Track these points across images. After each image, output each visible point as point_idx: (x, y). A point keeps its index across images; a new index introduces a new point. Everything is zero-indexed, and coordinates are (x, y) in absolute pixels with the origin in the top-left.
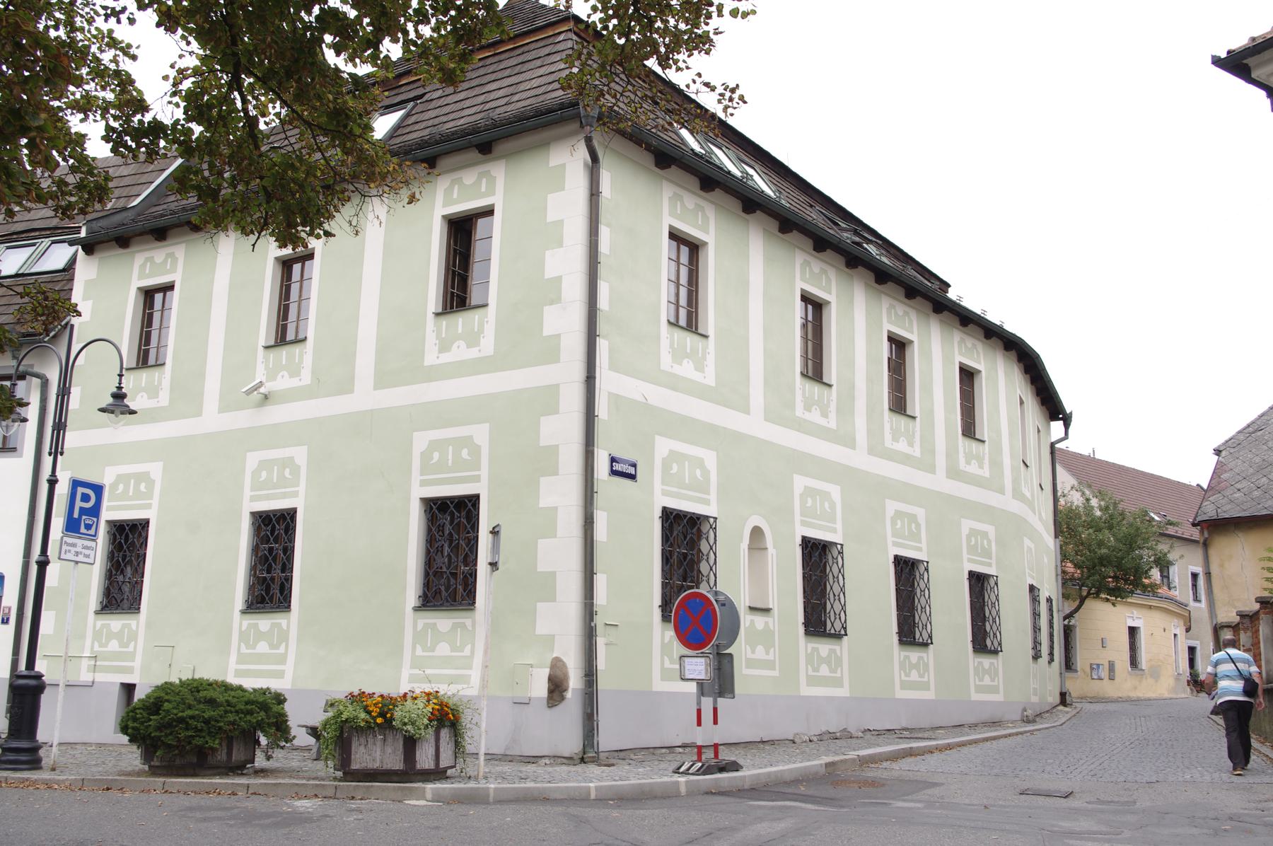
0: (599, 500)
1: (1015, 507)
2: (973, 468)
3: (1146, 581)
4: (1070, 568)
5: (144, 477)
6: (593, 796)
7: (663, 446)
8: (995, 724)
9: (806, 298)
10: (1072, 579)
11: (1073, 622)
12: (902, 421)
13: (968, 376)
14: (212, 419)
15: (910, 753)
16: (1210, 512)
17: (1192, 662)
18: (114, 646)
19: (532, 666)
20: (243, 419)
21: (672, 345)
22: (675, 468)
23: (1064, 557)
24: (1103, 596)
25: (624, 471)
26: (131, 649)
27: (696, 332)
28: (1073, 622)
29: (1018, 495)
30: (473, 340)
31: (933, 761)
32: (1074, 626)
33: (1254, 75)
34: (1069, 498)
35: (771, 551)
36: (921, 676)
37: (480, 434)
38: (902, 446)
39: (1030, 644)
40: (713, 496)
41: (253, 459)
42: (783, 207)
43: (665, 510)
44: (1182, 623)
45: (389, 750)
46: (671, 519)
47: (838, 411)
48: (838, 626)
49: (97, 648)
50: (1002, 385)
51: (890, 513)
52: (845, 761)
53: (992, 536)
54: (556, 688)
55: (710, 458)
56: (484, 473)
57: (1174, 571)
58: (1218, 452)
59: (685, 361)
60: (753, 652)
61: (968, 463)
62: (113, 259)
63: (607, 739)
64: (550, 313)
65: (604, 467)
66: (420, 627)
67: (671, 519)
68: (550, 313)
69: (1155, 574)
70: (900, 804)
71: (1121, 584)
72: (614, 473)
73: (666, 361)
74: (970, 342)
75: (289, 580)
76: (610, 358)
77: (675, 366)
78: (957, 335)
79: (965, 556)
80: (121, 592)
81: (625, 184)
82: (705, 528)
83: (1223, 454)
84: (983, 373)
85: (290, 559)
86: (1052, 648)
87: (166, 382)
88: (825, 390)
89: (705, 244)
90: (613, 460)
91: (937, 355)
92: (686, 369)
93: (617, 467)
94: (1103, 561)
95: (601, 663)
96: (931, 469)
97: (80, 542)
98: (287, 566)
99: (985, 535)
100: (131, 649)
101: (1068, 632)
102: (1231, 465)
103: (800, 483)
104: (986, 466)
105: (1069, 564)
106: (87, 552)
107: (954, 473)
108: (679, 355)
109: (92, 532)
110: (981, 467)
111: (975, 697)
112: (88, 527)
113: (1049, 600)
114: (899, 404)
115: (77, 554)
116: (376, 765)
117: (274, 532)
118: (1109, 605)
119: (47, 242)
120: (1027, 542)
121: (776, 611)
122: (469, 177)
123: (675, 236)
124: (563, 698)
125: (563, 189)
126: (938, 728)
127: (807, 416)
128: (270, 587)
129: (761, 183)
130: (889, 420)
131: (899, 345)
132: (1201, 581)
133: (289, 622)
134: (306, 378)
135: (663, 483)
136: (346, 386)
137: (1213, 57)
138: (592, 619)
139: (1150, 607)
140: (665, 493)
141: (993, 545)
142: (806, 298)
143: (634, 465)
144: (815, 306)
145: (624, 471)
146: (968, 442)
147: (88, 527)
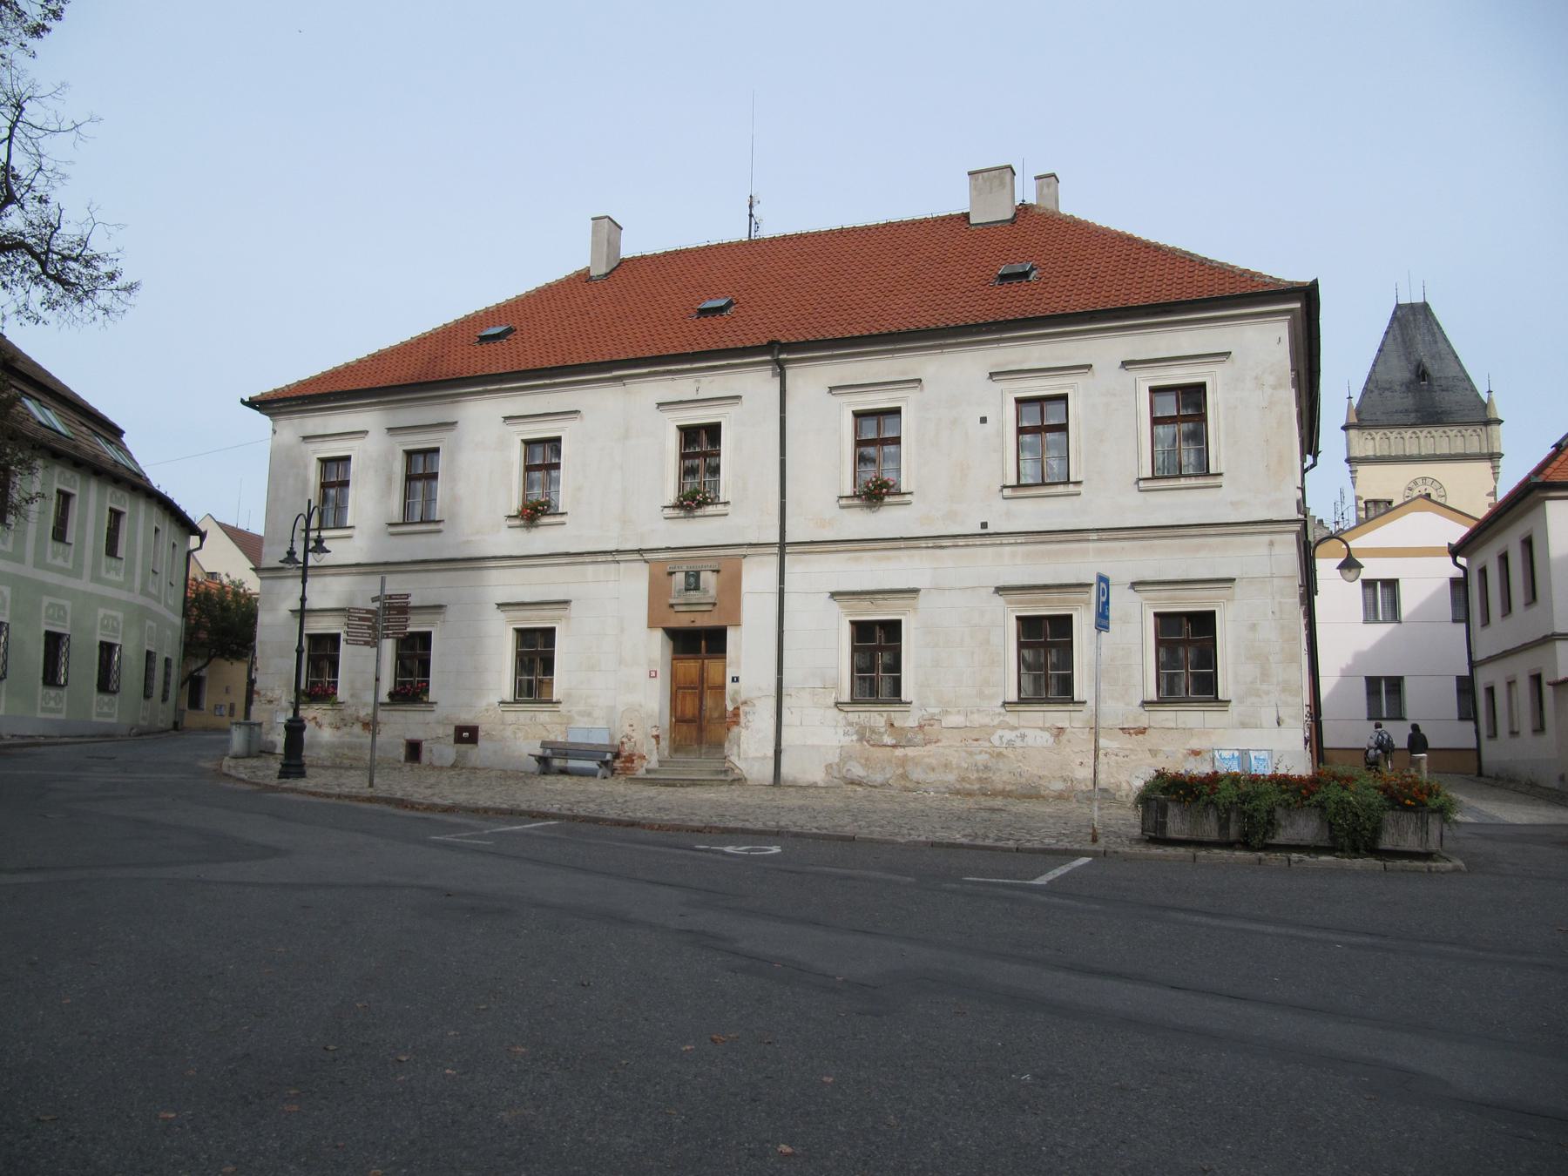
11: (203, 673)
12: (61, 546)
38: (59, 562)
74: (119, 493)
99: (115, 618)
111: (95, 718)
130: (104, 559)
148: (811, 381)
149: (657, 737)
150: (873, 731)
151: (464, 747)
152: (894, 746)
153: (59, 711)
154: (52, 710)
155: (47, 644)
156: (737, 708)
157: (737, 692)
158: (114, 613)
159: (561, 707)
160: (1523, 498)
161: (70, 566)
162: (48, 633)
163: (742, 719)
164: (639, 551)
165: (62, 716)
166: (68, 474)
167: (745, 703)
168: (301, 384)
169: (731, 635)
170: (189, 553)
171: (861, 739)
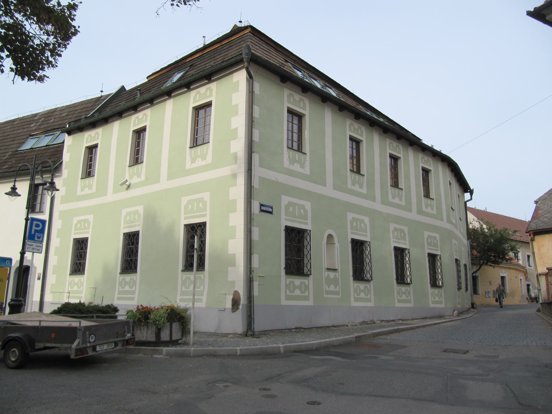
0: (254, 222)
1: (447, 226)
2: (429, 210)
3: (507, 258)
4: (475, 252)
5: (86, 221)
6: (239, 353)
7: (285, 200)
8: (440, 317)
9: (352, 139)
10: (476, 257)
11: (477, 274)
12: (397, 190)
13: (426, 172)
14: (111, 197)
15: (398, 331)
16: (533, 227)
17: (528, 290)
18: (75, 288)
19: (226, 294)
20: (125, 195)
21: (289, 157)
22: (291, 209)
23: (472, 248)
24: (489, 264)
25: (266, 209)
26: (81, 289)
27: (301, 152)
28: (477, 274)
29: (449, 221)
30: (204, 158)
31: (407, 334)
32: (478, 276)
33: (547, 18)
34: (473, 225)
35: (337, 244)
36: (407, 297)
38: (397, 201)
39: (456, 283)
40: (309, 221)
41: (124, 212)
42: (340, 100)
43: (286, 226)
44: (523, 274)
45: (149, 332)
46: (290, 231)
47: (367, 186)
48: (368, 276)
49: (70, 289)
50: (440, 176)
51: (391, 229)
52: (366, 335)
53: (438, 238)
54: (235, 303)
55: (308, 205)
56: (208, 213)
57: (520, 255)
58: (536, 202)
59: (295, 164)
60: (329, 287)
61: (427, 208)
62: (78, 136)
63: (258, 326)
64: (233, 143)
65: (258, 208)
66: (184, 278)
67: (290, 231)
68: (233, 143)
69: (511, 254)
70: (383, 357)
71: (497, 259)
72: (262, 211)
73: (286, 164)
74: (426, 158)
75: (136, 260)
76: (260, 161)
77: (291, 166)
78: (420, 155)
79: (426, 247)
81: (265, 87)
82: (306, 235)
83: (539, 203)
84: (433, 171)
85: (137, 251)
86: (467, 285)
87: (95, 183)
88: (361, 177)
89: (304, 115)
90: (261, 205)
91: (411, 164)
92: (296, 167)
93: (263, 208)
94: (490, 249)
95: (256, 293)
96: (410, 210)
97: (35, 244)
99: (435, 238)
100: (81, 289)
101: (475, 279)
102: (542, 207)
103: (350, 216)
104: (435, 209)
105: (475, 252)
106: (38, 248)
107: (420, 212)
108: (292, 161)
109: (41, 240)
110: (432, 209)
111: (432, 305)
112: (39, 238)
113: (465, 265)
114: (395, 184)
115: (33, 249)
116: (144, 339)
118: (492, 268)
119: (59, 132)
120: (454, 241)
121: (339, 270)
122: (202, 90)
123: (290, 112)
124: (238, 308)
125: (238, 91)
126: (415, 319)
127: (353, 188)
128: (129, 264)
129: (333, 92)
130: (391, 190)
131: (395, 159)
132: (531, 258)
133: (136, 277)
134: (143, 178)
135: (286, 215)
136: (157, 180)
137: (527, 12)
138: (251, 274)
139: (510, 268)
140: (286, 220)
141: (439, 242)
142: (352, 139)
143: (272, 208)
144: (356, 142)
145: (266, 209)
146: (426, 199)
147: (39, 238)
153: (307, 298)
154: (363, 300)
155: (396, 256)
160: (272, 331)
161: (403, 203)
165: (411, 305)
166: (395, 144)
170: (465, 203)
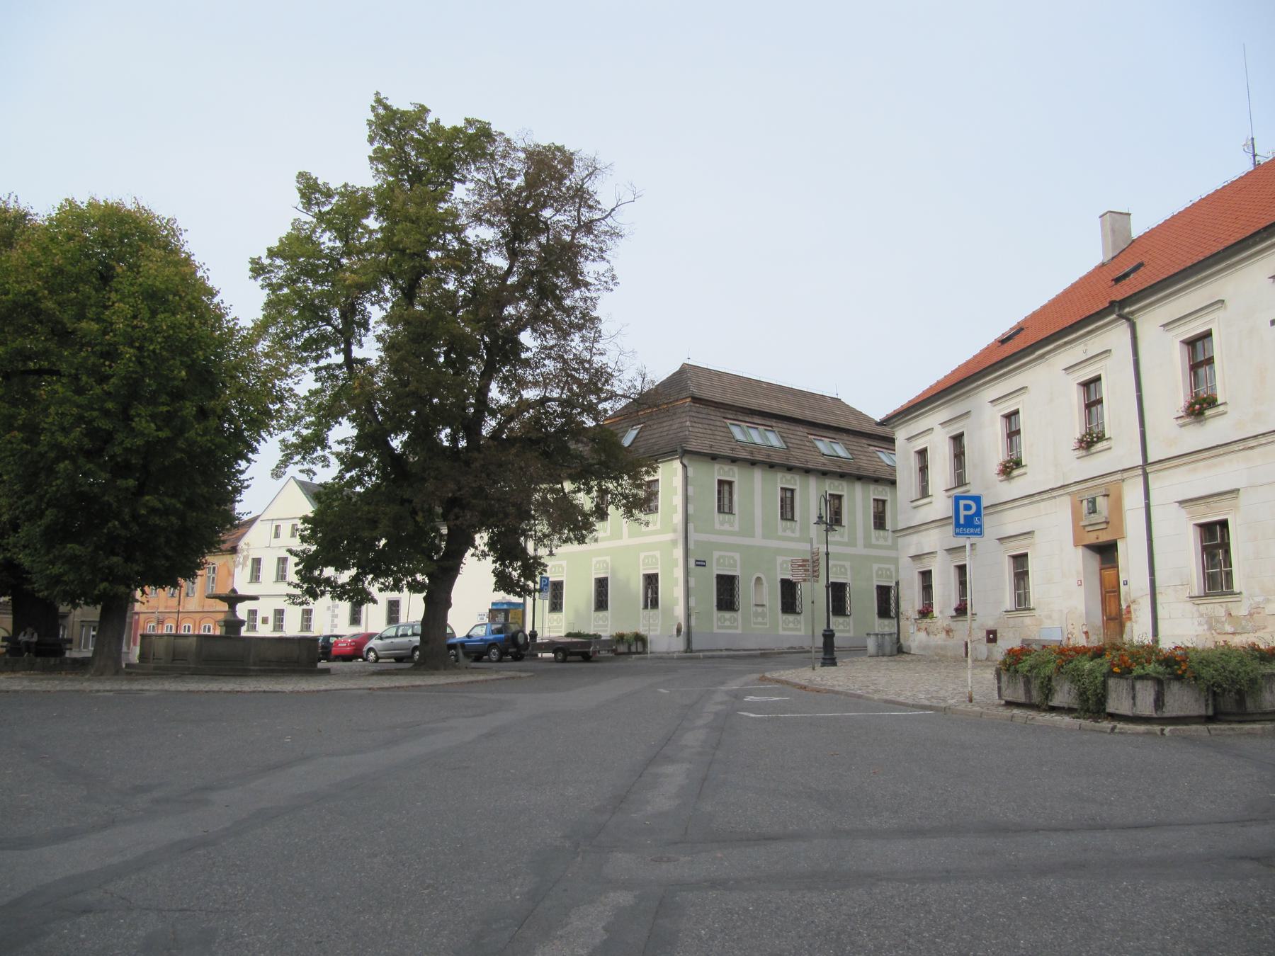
0: (691, 574)
7: (716, 554)
37: (658, 554)
54: (679, 631)
63: (695, 646)
65: (695, 562)
80: (556, 606)
98: (561, 598)
111: (781, 632)
117: (602, 584)
128: (601, 603)
145: (701, 563)
148: (1151, 321)
149: (1086, 633)
150: (1217, 621)
151: (991, 645)
152: (1233, 634)
156: (1129, 607)
157: (1128, 593)
158: (887, 566)
159: (1034, 613)
161: (846, 539)
162: (879, 587)
163: (1133, 616)
164: (1062, 487)
167: (1134, 602)
168: (924, 393)
169: (1121, 546)
171: (1211, 628)
